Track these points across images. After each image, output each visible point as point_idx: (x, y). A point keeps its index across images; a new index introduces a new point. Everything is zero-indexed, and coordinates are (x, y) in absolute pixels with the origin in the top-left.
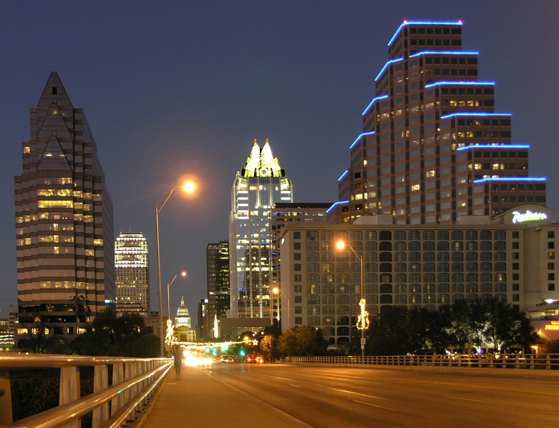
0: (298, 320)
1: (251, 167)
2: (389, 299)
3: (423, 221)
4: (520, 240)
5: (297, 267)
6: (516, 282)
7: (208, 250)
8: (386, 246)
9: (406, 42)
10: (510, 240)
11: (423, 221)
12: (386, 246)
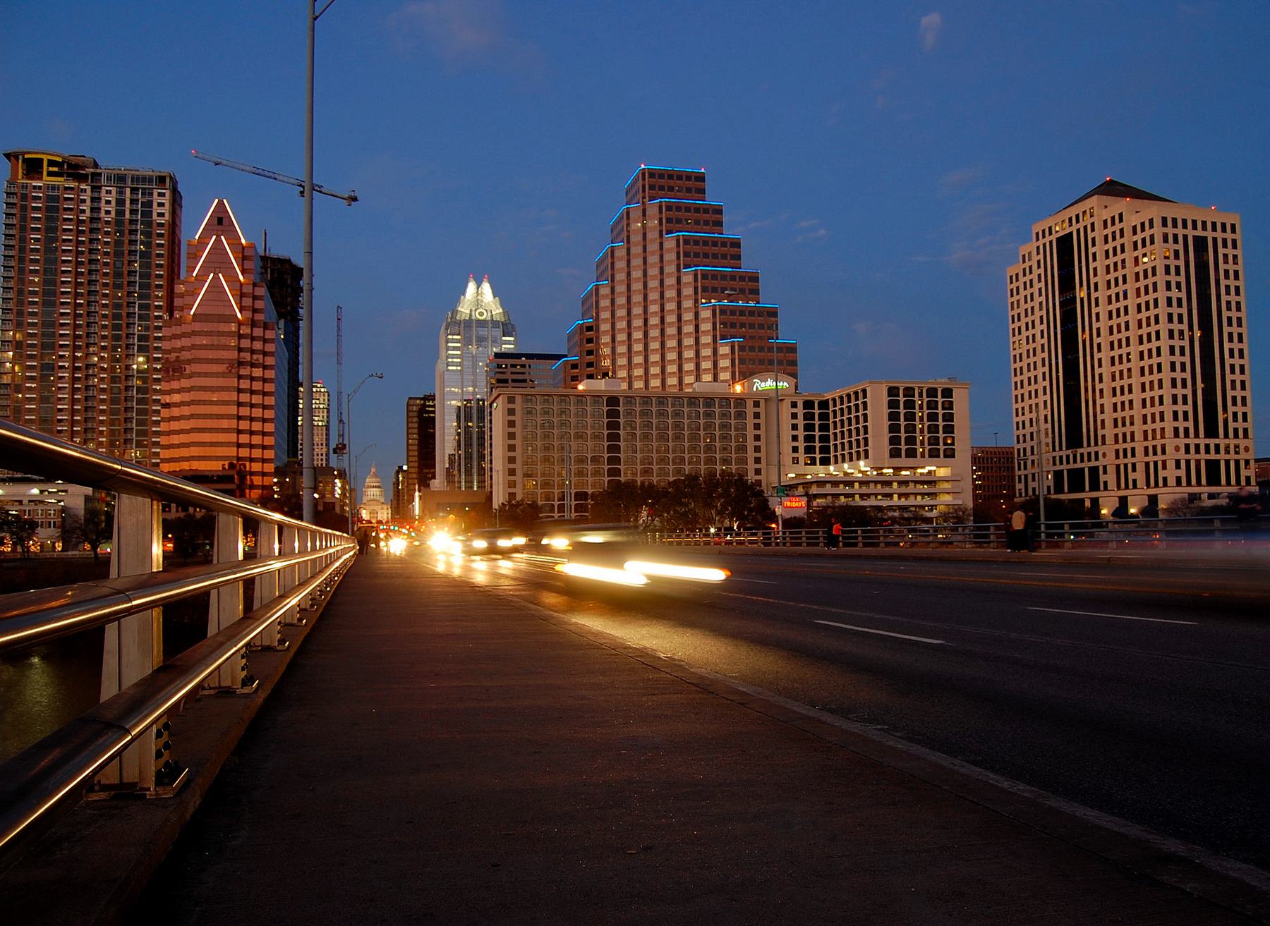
0: (512, 495)
1: (464, 309)
2: (616, 472)
3: (630, 386)
4: (761, 410)
5: (511, 436)
6: (758, 455)
7: (408, 405)
8: (613, 414)
9: (644, 186)
10: (750, 409)
11: (630, 386)
12: (613, 414)
